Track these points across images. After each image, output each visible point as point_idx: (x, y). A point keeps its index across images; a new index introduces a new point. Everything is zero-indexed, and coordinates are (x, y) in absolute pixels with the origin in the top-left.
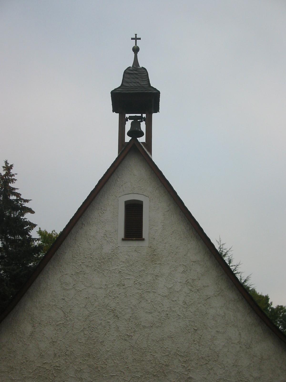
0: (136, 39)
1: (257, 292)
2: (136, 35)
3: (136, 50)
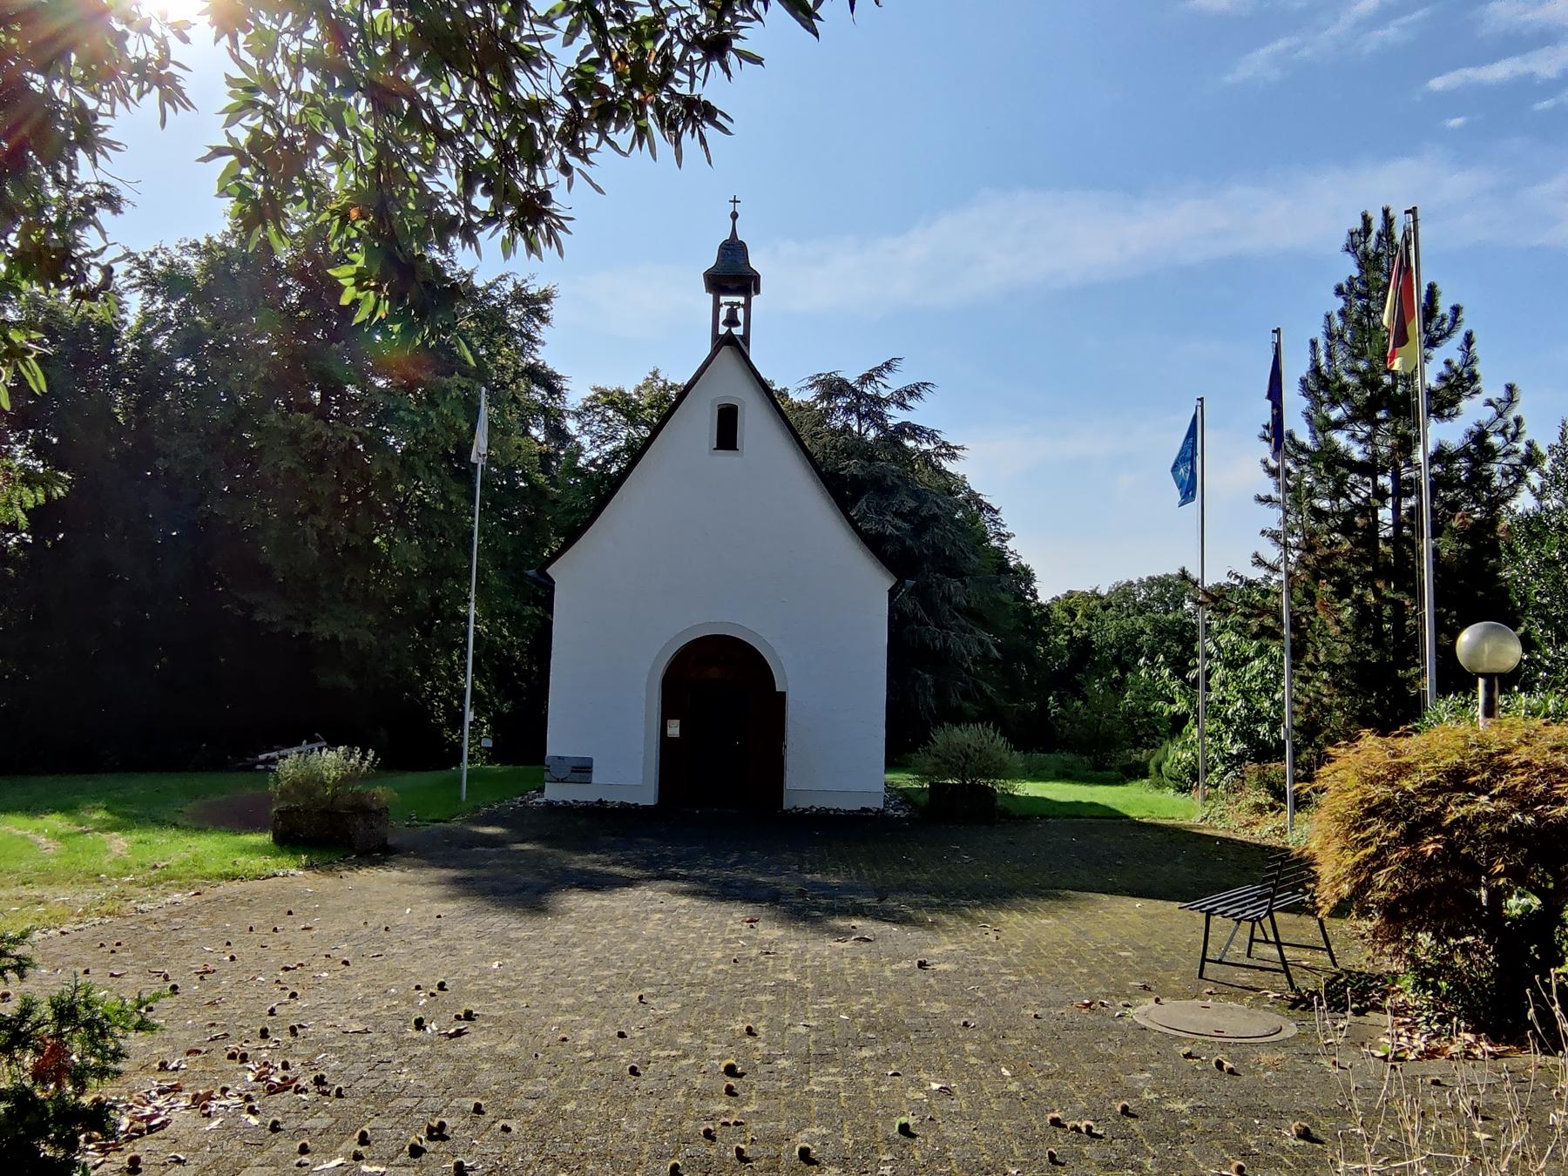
3: (735, 216)
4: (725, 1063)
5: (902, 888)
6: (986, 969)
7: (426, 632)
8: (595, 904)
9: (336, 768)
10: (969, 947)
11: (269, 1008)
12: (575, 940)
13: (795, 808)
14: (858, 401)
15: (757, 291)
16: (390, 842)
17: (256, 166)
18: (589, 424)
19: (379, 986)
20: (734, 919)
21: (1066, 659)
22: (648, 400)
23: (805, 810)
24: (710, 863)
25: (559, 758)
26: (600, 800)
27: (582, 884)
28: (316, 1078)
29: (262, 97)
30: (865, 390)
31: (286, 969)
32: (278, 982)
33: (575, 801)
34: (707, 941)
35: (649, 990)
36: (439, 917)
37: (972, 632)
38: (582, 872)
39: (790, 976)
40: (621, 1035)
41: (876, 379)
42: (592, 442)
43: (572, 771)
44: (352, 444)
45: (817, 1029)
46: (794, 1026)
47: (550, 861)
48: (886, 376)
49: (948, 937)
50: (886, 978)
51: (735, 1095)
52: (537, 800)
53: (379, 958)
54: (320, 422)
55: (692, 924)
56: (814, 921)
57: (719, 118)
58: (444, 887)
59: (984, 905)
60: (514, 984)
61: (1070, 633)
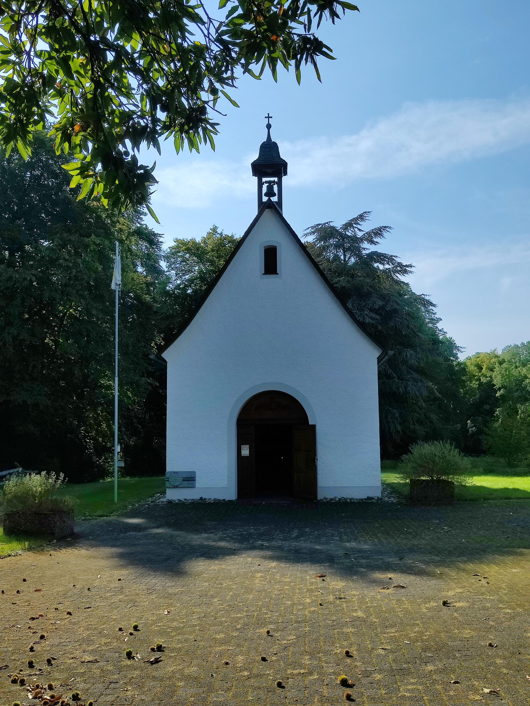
0: (269, 117)
1: (489, 563)
2: (268, 114)
3: (269, 126)
4: (340, 678)
5: (412, 550)
6: (489, 605)
7: (80, 396)
8: (216, 568)
9: (41, 485)
10: (471, 590)
11: (30, 647)
12: (212, 593)
13: (325, 498)
14: (343, 240)
15: (286, 174)
16: (77, 529)
17: (10, 101)
18: (174, 263)
19: (95, 629)
20: (309, 575)
21: (477, 396)
22: (211, 247)
23: (331, 499)
24: (281, 536)
25: (175, 472)
26: (202, 498)
27: (205, 554)
28: (73, 696)
29: (13, 57)
30: (347, 233)
31: (33, 619)
32: (30, 628)
33: (185, 499)
34: (297, 591)
35: (272, 626)
36: (120, 580)
37: (421, 381)
38: (201, 546)
39: (360, 614)
40: (264, 659)
41: (354, 225)
42: (176, 274)
43: (183, 480)
44: (31, 282)
45: (392, 651)
46: (376, 650)
47: (179, 539)
48: (361, 223)
49: (456, 583)
50: (424, 613)
51: (353, 700)
52: (161, 500)
53: (89, 610)
54: (11, 269)
55: (283, 579)
56: (363, 576)
57: (324, 49)
58: (117, 559)
59: (470, 560)
60: (182, 625)
61: (479, 380)
